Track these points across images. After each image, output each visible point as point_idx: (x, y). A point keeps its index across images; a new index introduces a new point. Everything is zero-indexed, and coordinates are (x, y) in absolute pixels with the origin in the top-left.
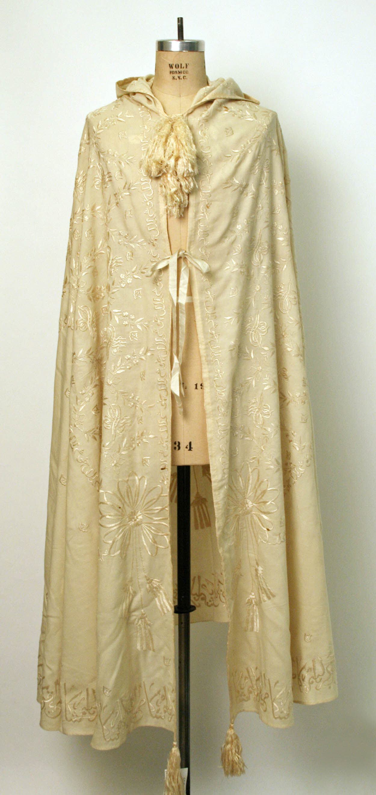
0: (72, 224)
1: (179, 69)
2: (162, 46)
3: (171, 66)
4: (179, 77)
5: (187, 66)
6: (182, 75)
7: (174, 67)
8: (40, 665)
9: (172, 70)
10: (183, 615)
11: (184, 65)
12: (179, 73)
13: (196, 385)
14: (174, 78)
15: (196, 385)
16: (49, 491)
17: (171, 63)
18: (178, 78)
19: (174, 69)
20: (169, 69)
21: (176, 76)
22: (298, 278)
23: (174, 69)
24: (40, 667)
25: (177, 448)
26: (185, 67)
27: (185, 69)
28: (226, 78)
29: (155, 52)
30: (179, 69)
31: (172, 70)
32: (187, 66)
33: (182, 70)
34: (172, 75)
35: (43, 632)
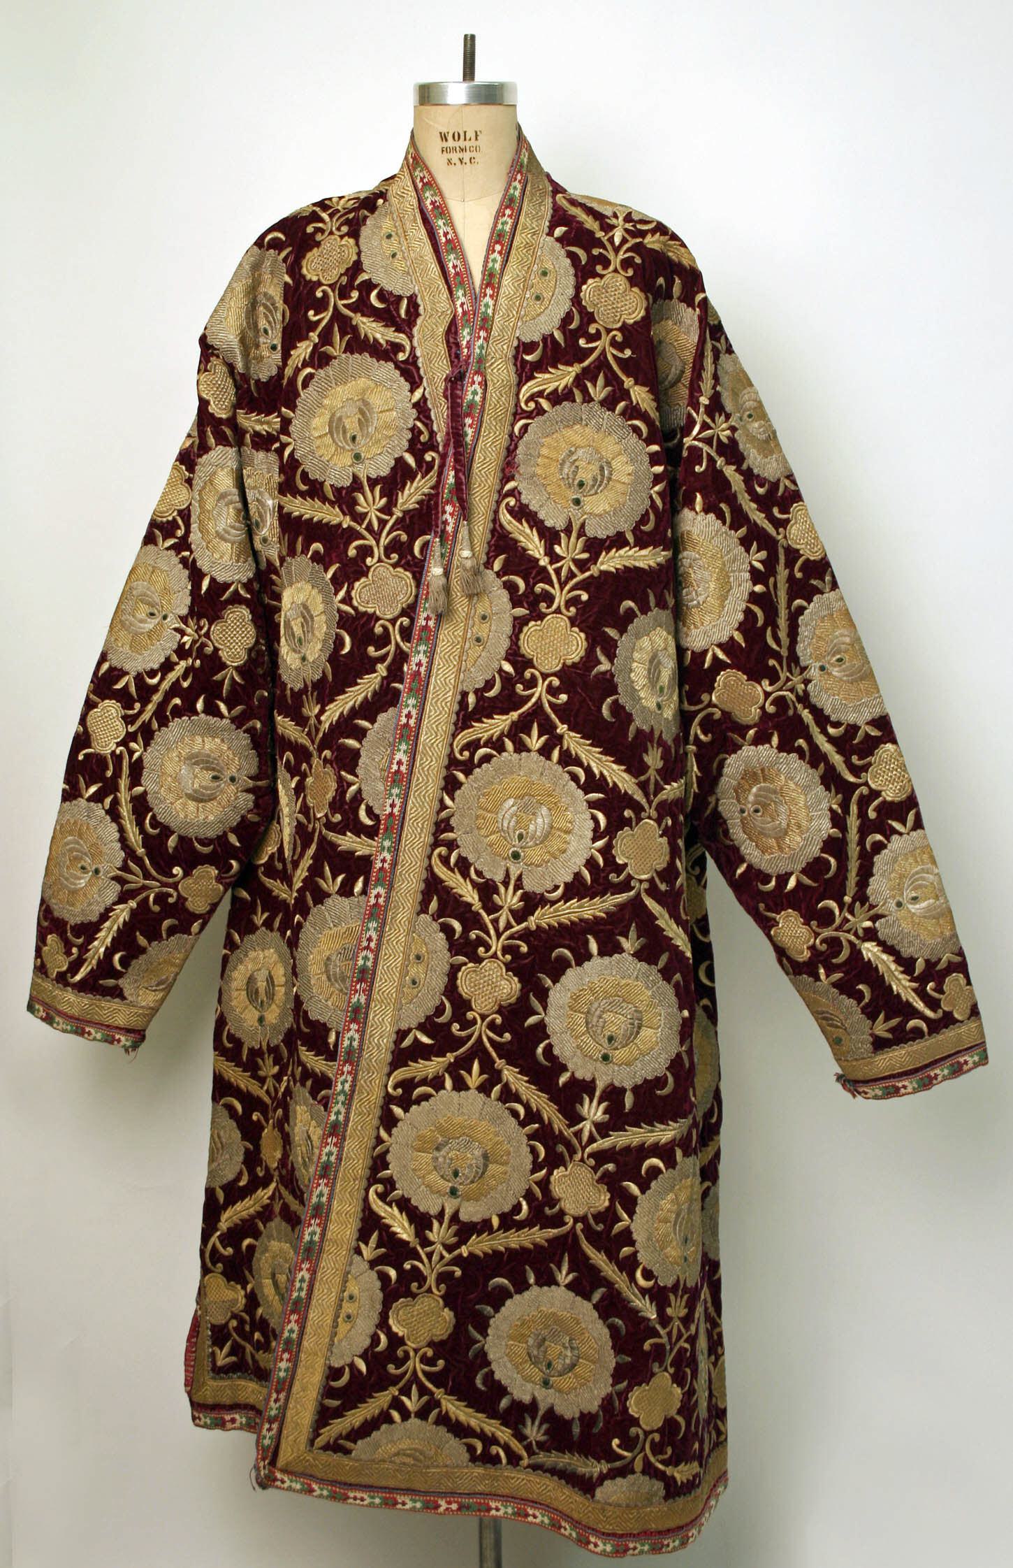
1: (462, 143)
3: (444, 137)
4: (461, 161)
6: (466, 156)
7: (450, 138)
9: (445, 145)
11: (471, 134)
14: (449, 162)
17: (444, 130)
18: (458, 162)
19: (451, 143)
20: (439, 144)
21: (455, 157)
23: (451, 143)
30: (462, 143)
33: (468, 144)
34: (447, 156)
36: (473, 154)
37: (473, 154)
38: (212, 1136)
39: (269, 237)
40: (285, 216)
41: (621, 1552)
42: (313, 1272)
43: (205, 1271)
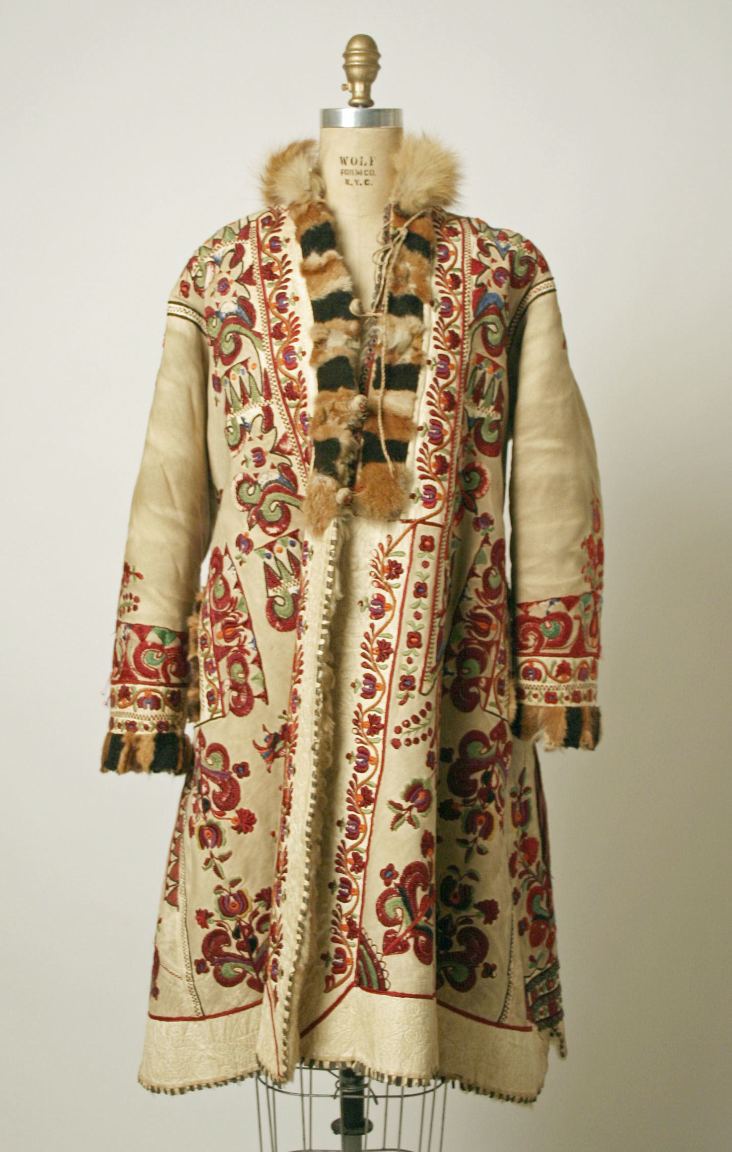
3: (344, 161)
4: (356, 181)
5: (372, 161)
7: (348, 162)
8: (492, 1095)
9: (344, 167)
10: (307, 1148)
12: (359, 173)
14: (347, 182)
17: (344, 155)
18: (354, 183)
19: (349, 166)
21: (352, 178)
22: (481, 1083)
23: (349, 166)
26: (369, 163)
27: (368, 167)
28: (460, 171)
31: (344, 167)
35: (225, 1083)
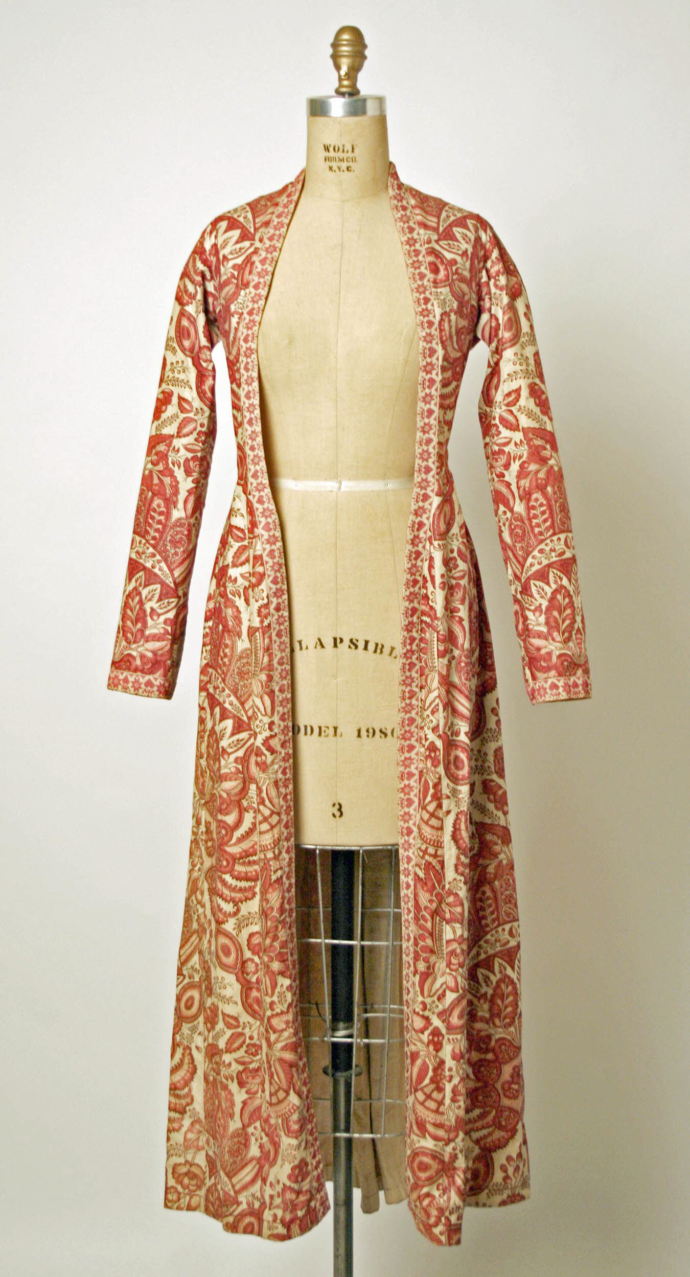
0: (187, 906)
1: (340, 155)
2: (317, 108)
3: (327, 149)
4: (339, 168)
5: (353, 149)
6: (344, 165)
7: (331, 149)
9: (327, 154)
11: (348, 147)
13: (359, 731)
14: (331, 168)
15: (359, 731)
16: (183, 641)
17: (327, 143)
18: (337, 170)
19: (332, 154)
20: (323, 154)
21: (334, 165)
23: (332, 154)
24: (356, 66)
25: (338, 814)
27: (350, 155)
29: (306, 118)
30: (340, 155)
32: (353, 149)
33: (345, 155)
34: (328, 164)
36: (350, 164)
37: (350, 164)
38: (197, 536)
39: (217, 571)
40: (525, 1089)
41: (489, 366)
42: (502, 541)
43: (166, 349)
